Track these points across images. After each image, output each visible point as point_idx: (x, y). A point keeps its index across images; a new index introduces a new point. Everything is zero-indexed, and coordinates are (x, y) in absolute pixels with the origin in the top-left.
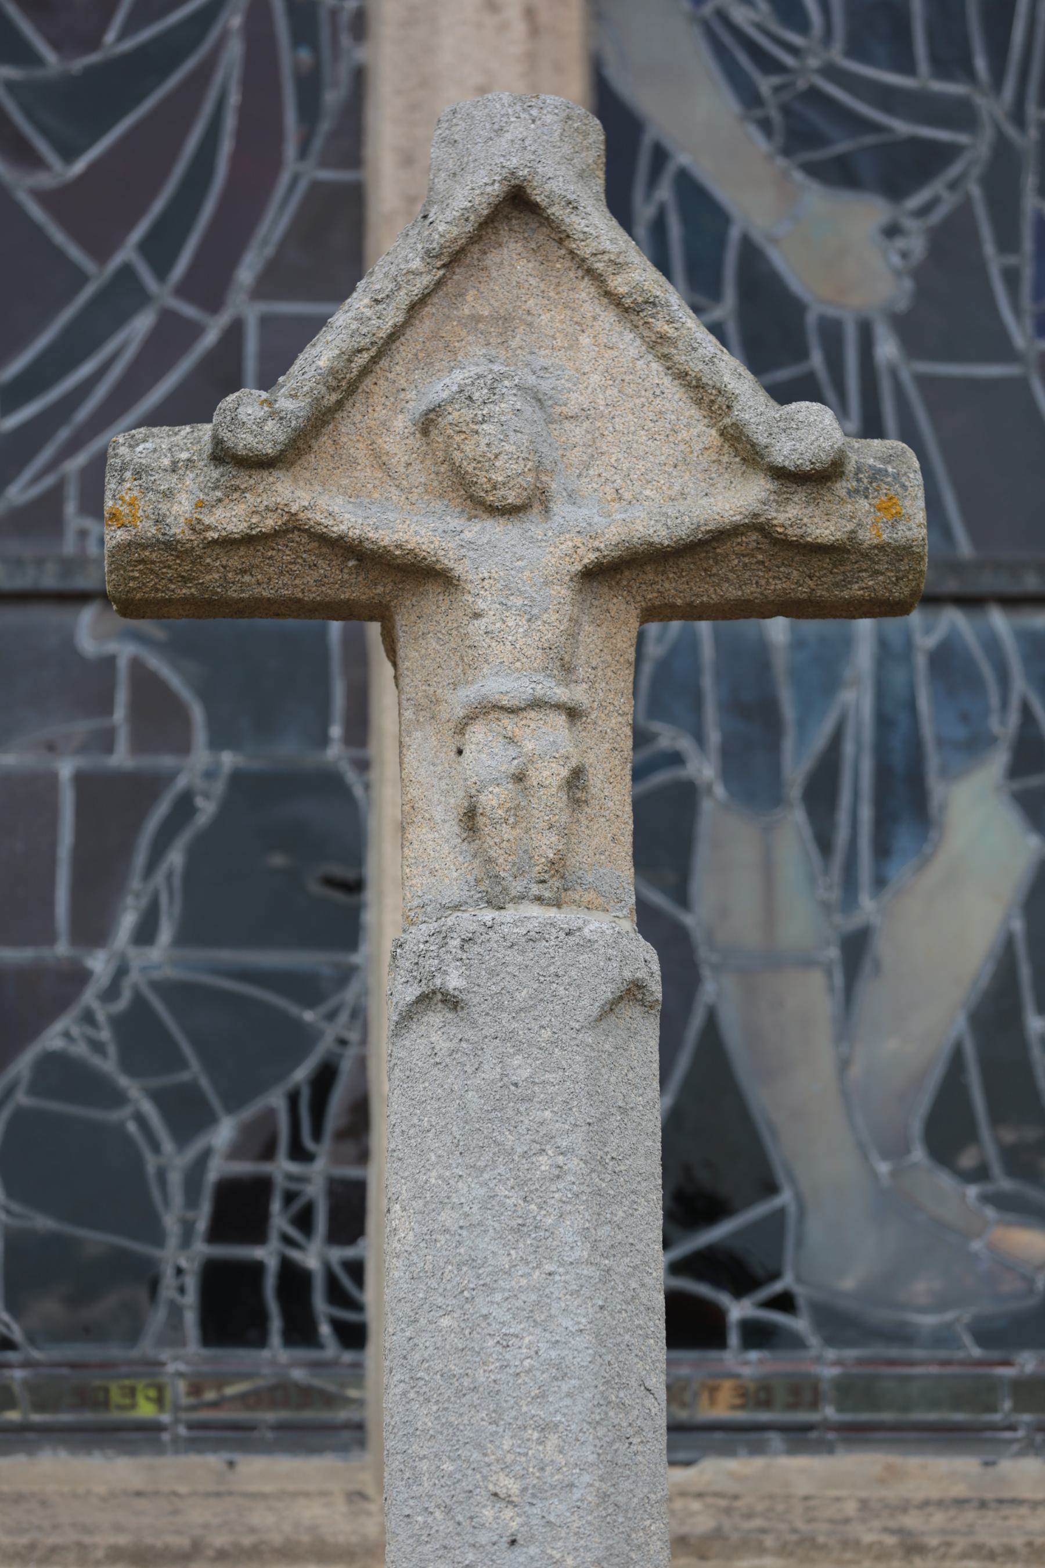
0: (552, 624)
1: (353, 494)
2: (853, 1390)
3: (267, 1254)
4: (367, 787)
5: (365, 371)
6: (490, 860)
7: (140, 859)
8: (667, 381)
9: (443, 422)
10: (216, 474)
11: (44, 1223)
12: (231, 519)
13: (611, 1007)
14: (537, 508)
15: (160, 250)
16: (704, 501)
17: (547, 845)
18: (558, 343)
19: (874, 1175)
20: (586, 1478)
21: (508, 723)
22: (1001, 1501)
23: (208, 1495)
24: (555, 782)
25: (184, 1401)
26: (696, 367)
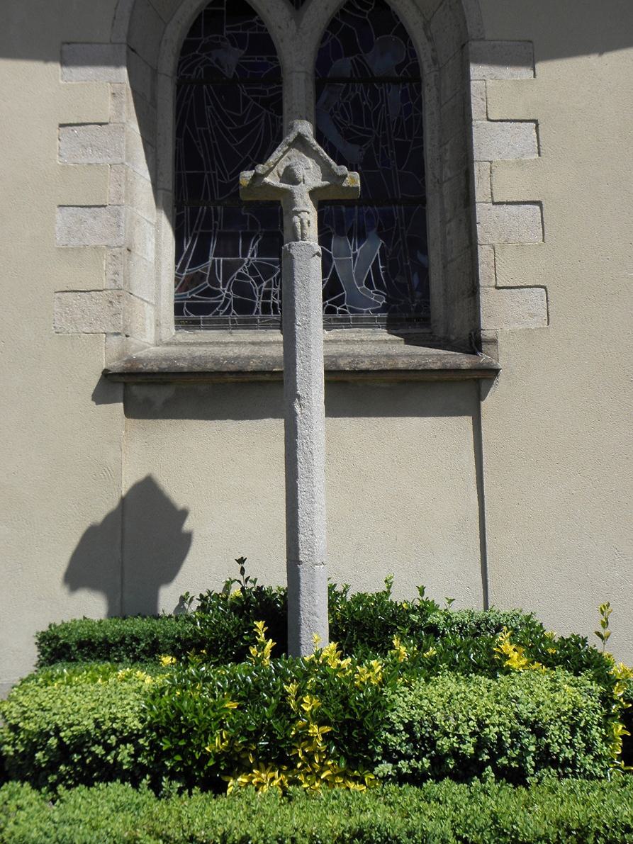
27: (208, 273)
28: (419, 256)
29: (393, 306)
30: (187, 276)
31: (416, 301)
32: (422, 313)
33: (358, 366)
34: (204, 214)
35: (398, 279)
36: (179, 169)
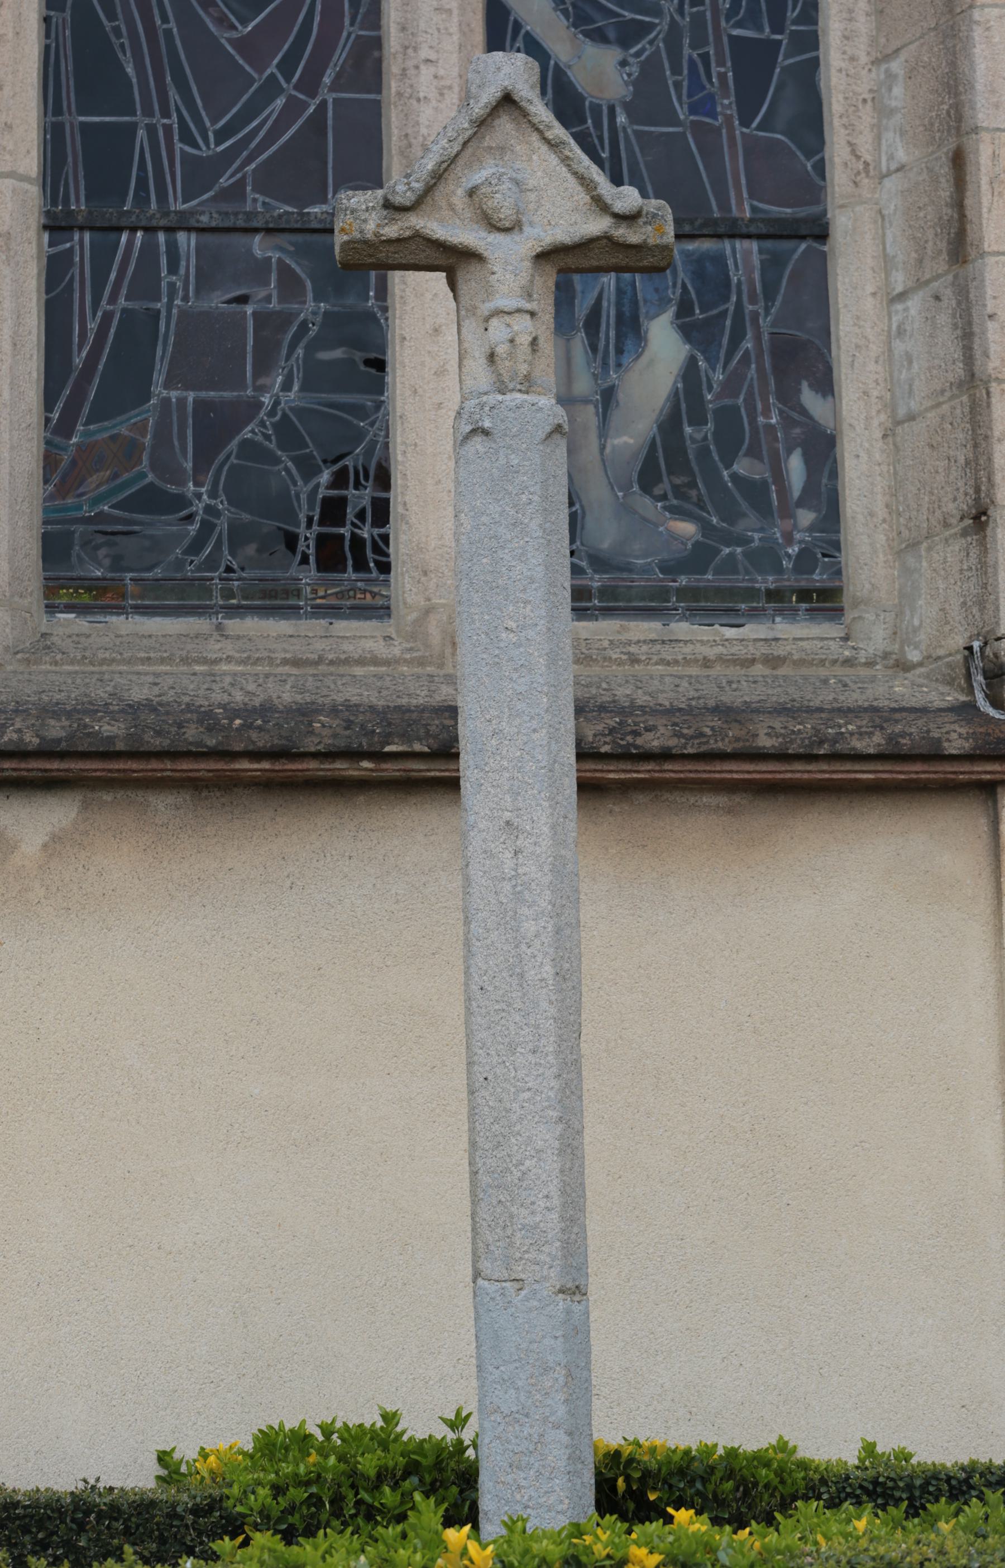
0: (524, 278)
1: (441, 221)
2: (606, 593)
3: (345, 531)
4: (387, 319)
5: (446, 170)
6: (500, 375)
7: (284, 352)
8: (569, 175)
9: (478, 193)
10: (385, 213)
11: (246, 517)
12: (391, 231)
13: (549, 435)
14: (517, 228)
15: (287, 67)
16: (585, 226)
17: (523, 369)
18: (524, 158)
19: (617, 496)
20: (542, 622)
21: (507, 319)
22: (671, 641)
23: (321, 637)
24: (527, 343)
25: (310, 596)
26: (581, 170)
27: (148, 440)
28: (809, 398)
29: (727, 550)
30: (78, 445)
31: (798, 536)
32: (815, 577)
33: (639, 741)
34: (136, 254)
35: (743, 466)
36: (58, 111)
